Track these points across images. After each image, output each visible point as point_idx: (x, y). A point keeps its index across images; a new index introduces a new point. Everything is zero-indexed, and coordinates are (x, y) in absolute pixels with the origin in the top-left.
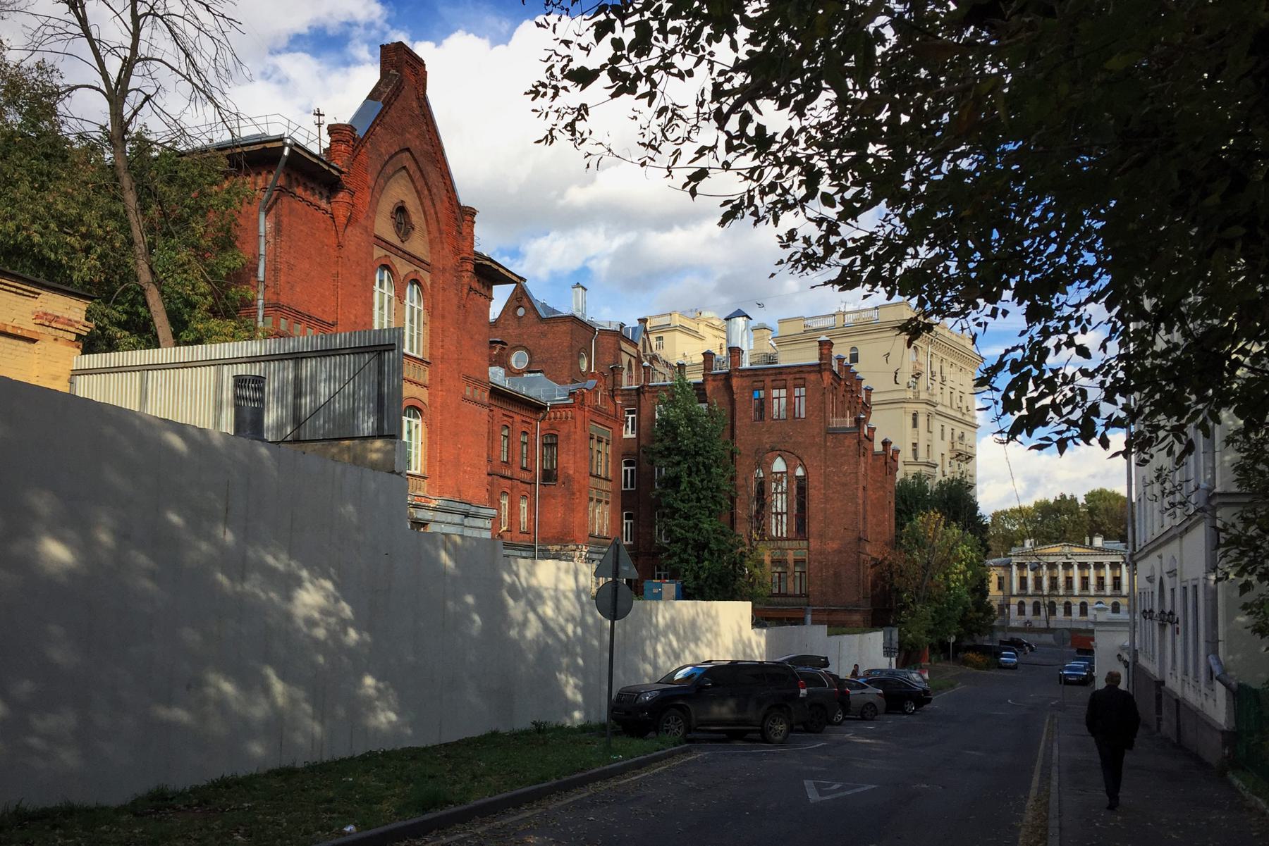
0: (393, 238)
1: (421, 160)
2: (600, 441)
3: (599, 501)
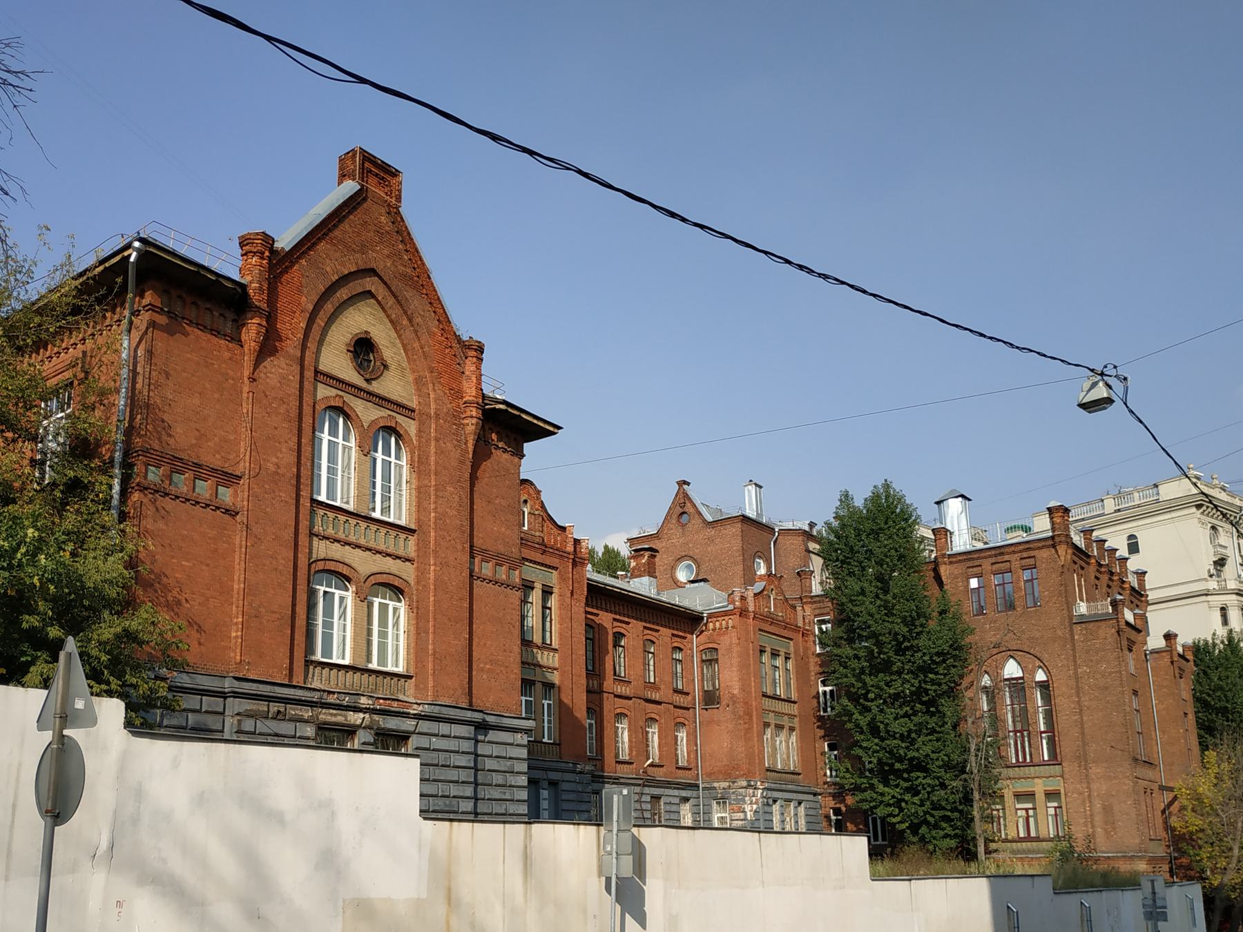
0: (357, 379)
1: (396, 284)
2: (775, 654)
3: (779, 727)
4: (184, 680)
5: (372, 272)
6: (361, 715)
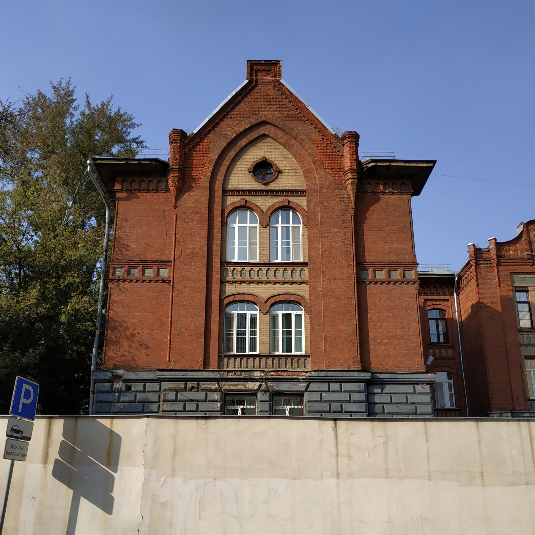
4: (132, 375)
5: (264, 123)
6: (258, 384)
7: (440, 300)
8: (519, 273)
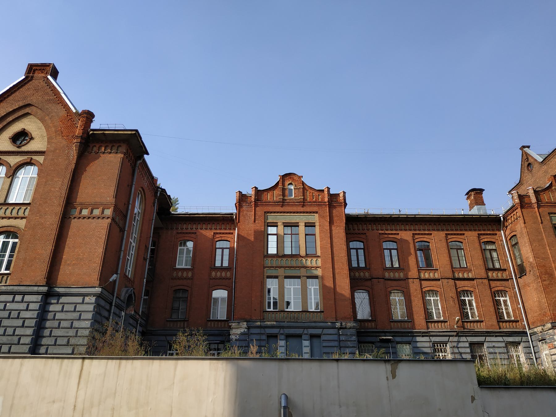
5: (29, 105)
7: (226, 233)
8: (271, 212)
